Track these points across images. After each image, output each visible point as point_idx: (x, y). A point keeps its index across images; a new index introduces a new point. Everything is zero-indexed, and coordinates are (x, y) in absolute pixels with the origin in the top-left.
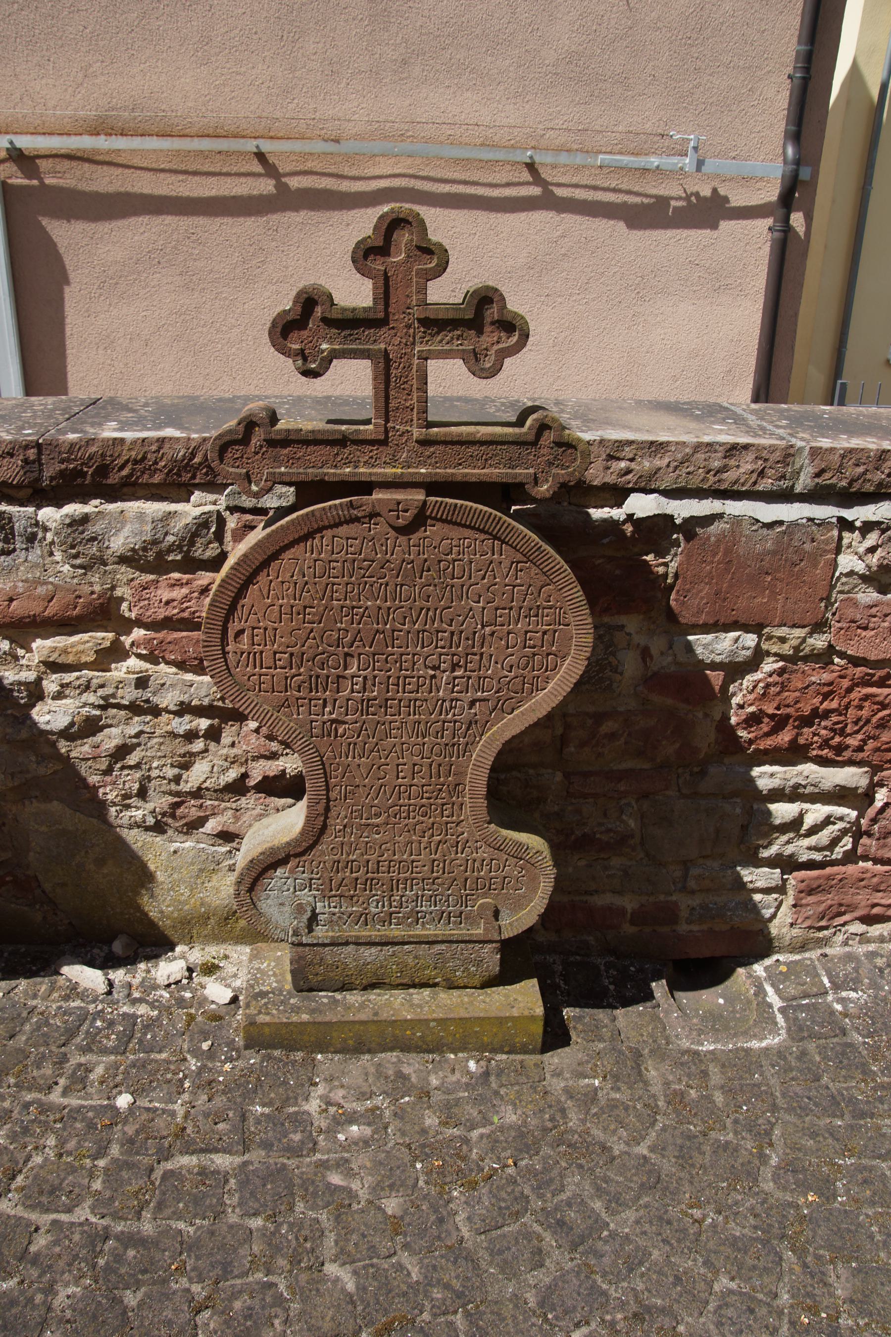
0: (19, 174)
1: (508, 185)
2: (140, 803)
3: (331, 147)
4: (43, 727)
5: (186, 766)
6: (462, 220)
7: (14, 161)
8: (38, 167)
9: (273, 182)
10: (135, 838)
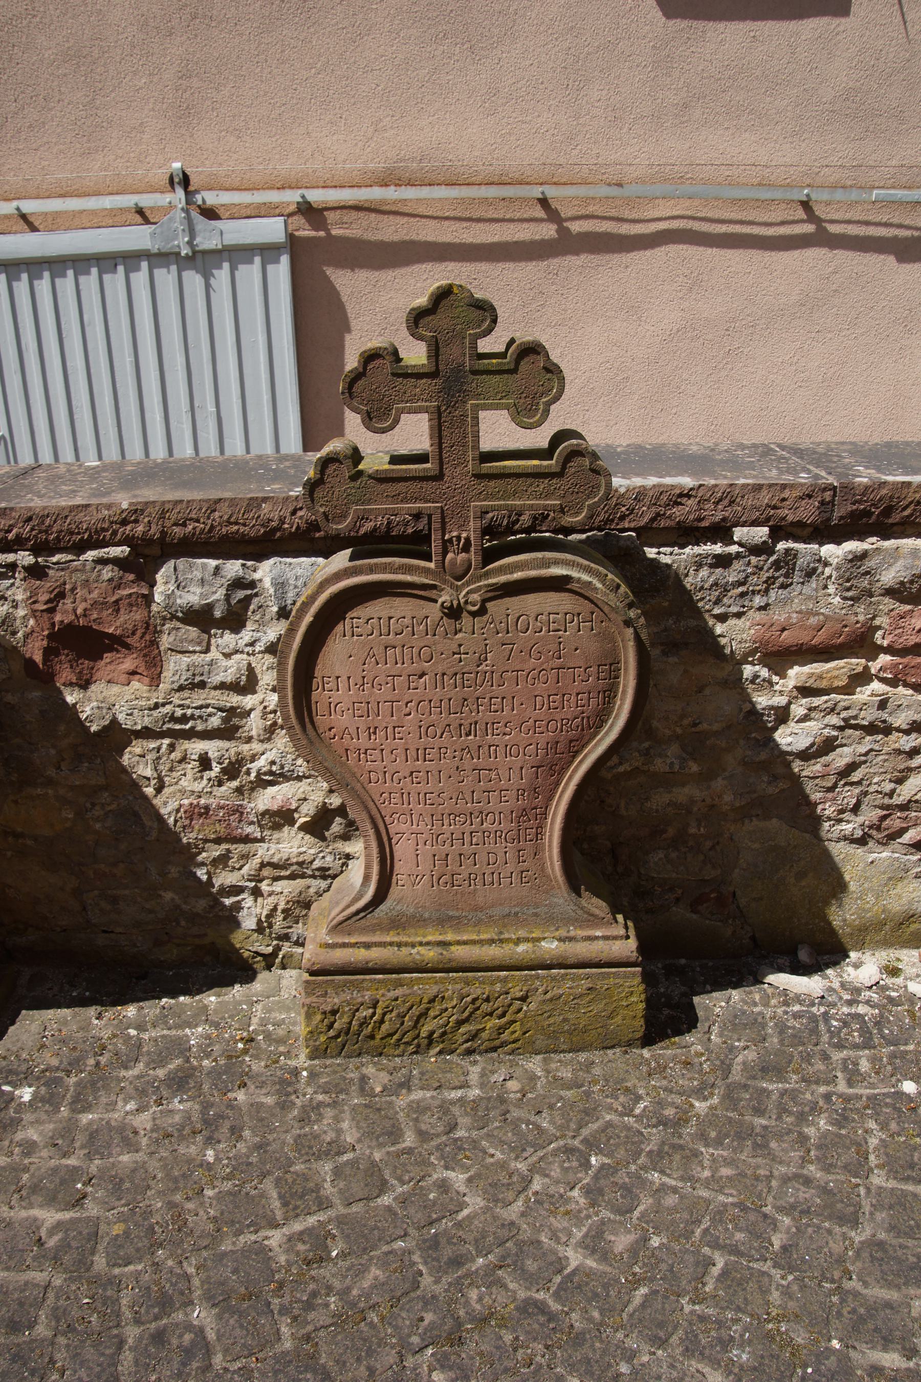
0: (307, 226)
1: (783, 223)
2: (852, 817)
3: (614, 191)
4: (785, 748)
5: (900, 781)
6: (738, 259)
7: (302, 214)
8: (326, 219)
9: (555, 227)
10: (839, 850)
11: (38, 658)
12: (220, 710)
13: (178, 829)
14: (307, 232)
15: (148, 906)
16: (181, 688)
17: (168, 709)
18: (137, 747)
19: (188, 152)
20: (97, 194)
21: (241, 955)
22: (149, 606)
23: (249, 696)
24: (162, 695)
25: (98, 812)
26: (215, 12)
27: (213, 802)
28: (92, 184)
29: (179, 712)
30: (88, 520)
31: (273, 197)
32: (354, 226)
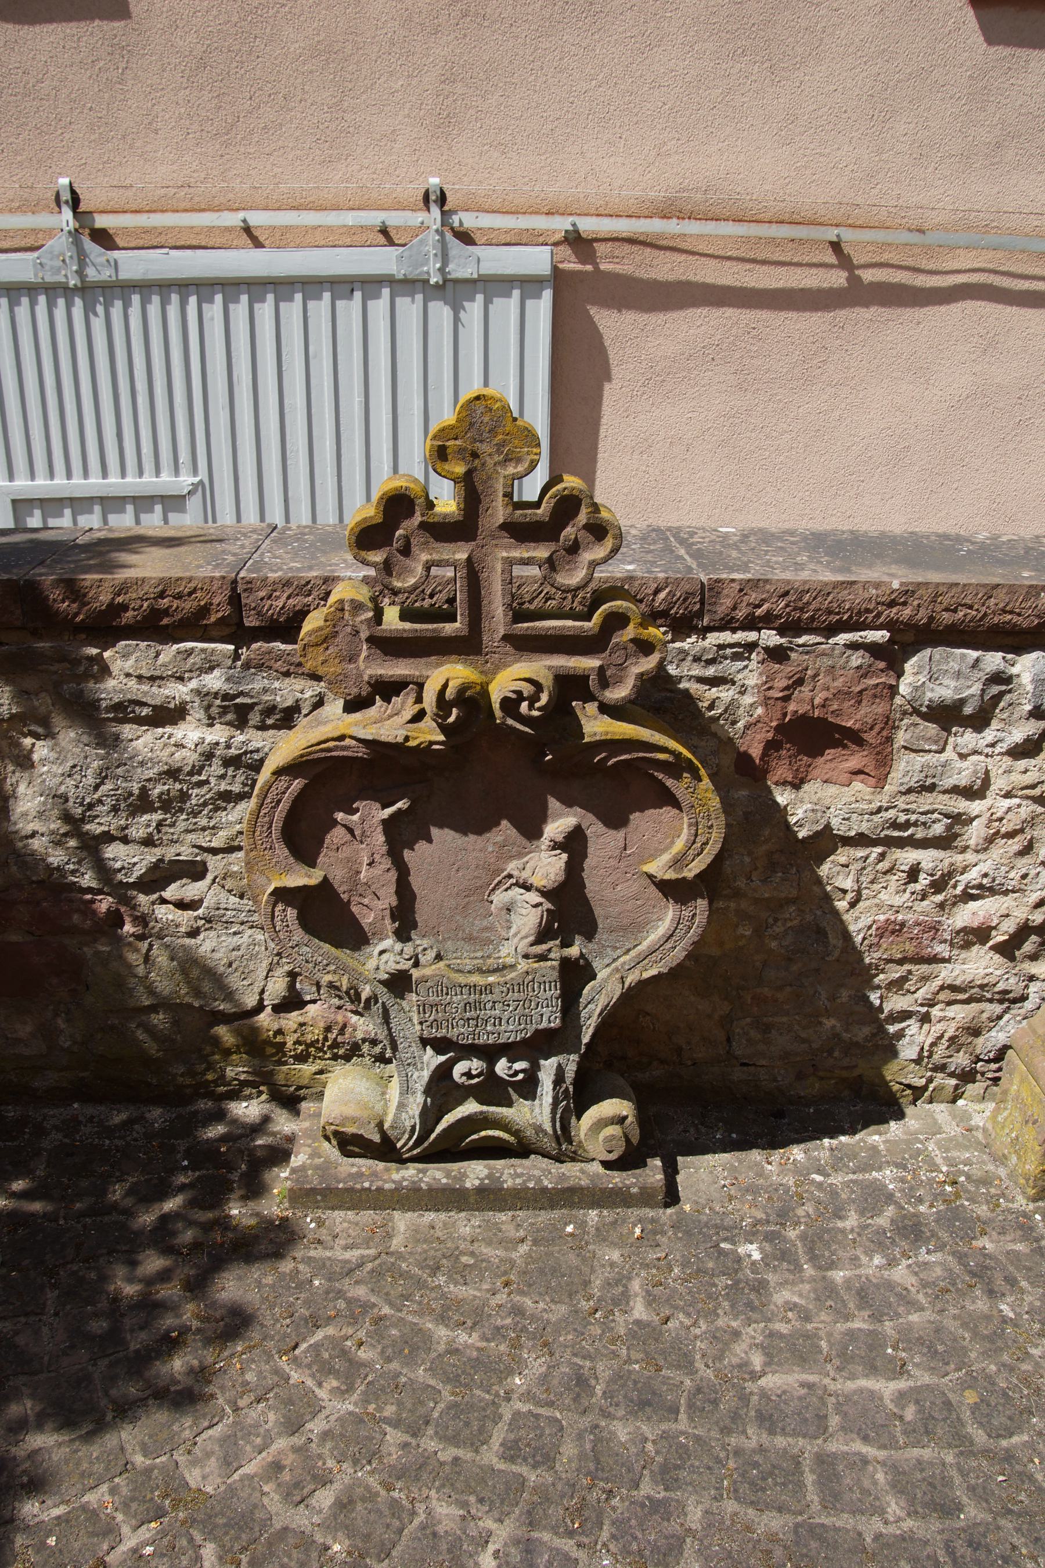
0: (573, 258)
3: (915, 238)
7: (569, 244)
8: (595, 252)
9: (845, 274)
11: (756, 752)
12: (947, 816)
13: (863, 949)
14: (572, 265)
15: (803, 1035)
16: (909, 791)
17: (891, 814)
18: (842, 855)
19: (445, 166)
20: (337, 208)
21: (889, 1088)
22: (892, 698)
23: (977, 802)
24: (886, 798)
25: (779, 929)
26: (488, 10)
27: (910, 918)
28: (330, 197)
29: (902, 818)
30: (851, 600)
31: (540, 223)
32: (626, 261)
